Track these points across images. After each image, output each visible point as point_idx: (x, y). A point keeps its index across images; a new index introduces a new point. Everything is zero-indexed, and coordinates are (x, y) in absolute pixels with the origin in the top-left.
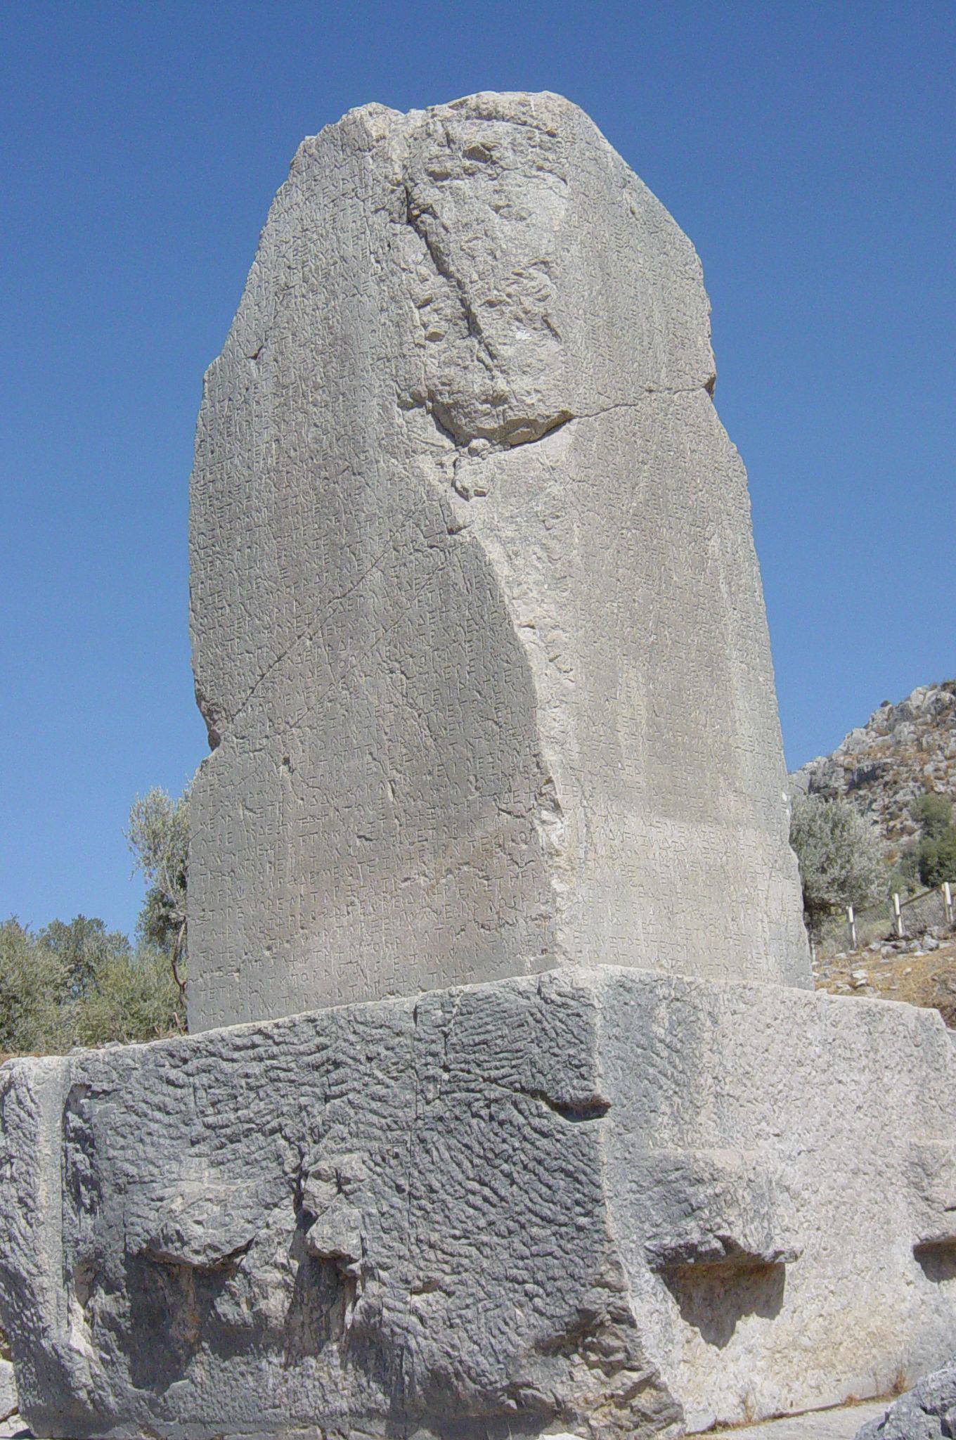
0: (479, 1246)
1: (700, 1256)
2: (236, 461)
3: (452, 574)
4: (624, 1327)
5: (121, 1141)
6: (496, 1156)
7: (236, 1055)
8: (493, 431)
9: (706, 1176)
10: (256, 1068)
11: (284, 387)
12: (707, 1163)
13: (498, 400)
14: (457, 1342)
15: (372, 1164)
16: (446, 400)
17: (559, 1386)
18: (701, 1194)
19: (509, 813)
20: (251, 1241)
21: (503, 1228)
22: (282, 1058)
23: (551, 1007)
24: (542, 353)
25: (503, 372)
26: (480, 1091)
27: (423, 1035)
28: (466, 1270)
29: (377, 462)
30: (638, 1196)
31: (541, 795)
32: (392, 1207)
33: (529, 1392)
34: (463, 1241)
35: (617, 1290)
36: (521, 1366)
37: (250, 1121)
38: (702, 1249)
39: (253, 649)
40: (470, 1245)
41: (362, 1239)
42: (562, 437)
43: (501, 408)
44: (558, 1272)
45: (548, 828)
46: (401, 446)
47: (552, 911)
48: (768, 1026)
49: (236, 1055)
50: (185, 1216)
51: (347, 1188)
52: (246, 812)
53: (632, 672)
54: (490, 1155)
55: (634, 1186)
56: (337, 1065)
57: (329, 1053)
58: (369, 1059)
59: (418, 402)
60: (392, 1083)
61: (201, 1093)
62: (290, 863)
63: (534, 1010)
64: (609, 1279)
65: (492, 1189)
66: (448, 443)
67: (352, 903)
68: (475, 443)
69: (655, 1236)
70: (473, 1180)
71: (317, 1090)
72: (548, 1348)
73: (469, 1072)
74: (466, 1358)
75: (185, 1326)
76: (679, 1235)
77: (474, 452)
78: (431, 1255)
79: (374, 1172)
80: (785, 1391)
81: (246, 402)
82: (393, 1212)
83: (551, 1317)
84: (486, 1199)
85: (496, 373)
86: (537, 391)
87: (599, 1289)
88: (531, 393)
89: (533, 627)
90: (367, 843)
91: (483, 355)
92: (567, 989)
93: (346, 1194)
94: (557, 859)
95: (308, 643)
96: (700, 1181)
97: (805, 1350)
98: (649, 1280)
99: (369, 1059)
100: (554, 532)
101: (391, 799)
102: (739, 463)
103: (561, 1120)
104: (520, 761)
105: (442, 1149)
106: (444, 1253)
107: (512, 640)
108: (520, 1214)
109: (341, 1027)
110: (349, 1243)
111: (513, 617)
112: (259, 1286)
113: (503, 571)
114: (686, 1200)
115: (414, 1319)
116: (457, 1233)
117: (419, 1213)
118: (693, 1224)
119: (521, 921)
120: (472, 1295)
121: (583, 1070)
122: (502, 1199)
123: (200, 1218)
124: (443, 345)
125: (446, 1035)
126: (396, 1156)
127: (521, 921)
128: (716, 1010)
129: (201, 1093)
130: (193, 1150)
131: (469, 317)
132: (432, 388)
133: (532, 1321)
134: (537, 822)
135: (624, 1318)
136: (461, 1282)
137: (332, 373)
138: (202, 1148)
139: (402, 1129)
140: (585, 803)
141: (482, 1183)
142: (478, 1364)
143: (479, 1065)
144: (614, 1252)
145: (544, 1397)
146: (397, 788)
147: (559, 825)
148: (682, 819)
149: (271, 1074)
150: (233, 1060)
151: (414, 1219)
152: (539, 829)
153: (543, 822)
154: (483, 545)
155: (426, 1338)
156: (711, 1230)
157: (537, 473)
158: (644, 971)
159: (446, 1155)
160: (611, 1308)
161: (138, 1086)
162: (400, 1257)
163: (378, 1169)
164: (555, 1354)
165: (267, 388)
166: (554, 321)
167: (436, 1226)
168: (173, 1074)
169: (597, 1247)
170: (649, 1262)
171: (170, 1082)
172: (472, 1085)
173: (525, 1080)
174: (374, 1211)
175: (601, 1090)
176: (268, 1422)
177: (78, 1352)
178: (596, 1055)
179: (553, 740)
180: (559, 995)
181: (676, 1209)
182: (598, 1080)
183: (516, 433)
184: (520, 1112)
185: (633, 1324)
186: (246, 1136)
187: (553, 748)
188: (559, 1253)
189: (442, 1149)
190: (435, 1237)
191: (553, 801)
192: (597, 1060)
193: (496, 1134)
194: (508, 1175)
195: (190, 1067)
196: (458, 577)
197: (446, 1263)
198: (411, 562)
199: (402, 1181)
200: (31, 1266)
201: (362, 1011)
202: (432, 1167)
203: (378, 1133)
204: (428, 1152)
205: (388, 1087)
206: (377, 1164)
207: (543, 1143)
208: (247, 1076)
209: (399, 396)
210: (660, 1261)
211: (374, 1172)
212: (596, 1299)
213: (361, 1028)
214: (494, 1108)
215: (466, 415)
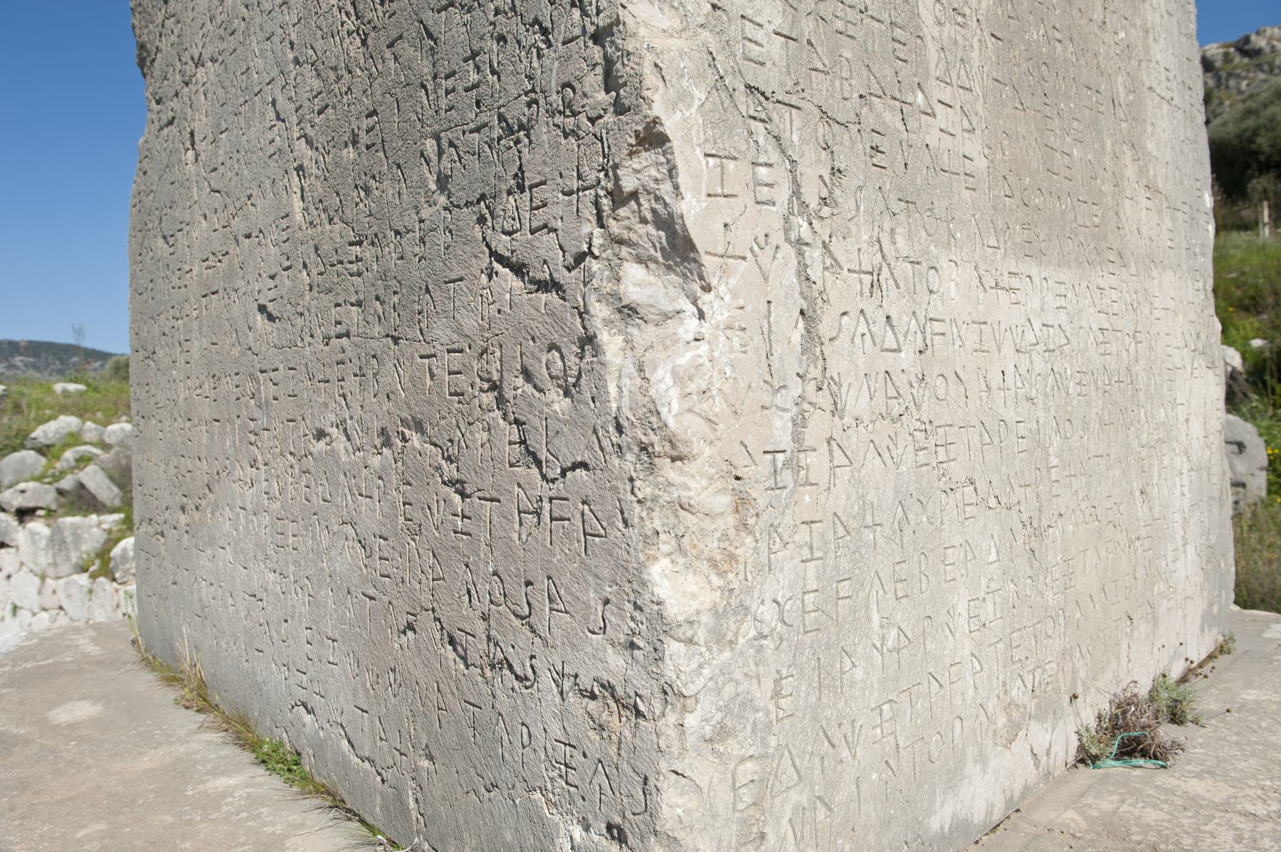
31: (619, 198)
45: (644, 335)
90: (269, 326)
94: (669, 471)
104: (552, 73)
134: (600, 311)
152: (611, 342)
153: (629, 312)
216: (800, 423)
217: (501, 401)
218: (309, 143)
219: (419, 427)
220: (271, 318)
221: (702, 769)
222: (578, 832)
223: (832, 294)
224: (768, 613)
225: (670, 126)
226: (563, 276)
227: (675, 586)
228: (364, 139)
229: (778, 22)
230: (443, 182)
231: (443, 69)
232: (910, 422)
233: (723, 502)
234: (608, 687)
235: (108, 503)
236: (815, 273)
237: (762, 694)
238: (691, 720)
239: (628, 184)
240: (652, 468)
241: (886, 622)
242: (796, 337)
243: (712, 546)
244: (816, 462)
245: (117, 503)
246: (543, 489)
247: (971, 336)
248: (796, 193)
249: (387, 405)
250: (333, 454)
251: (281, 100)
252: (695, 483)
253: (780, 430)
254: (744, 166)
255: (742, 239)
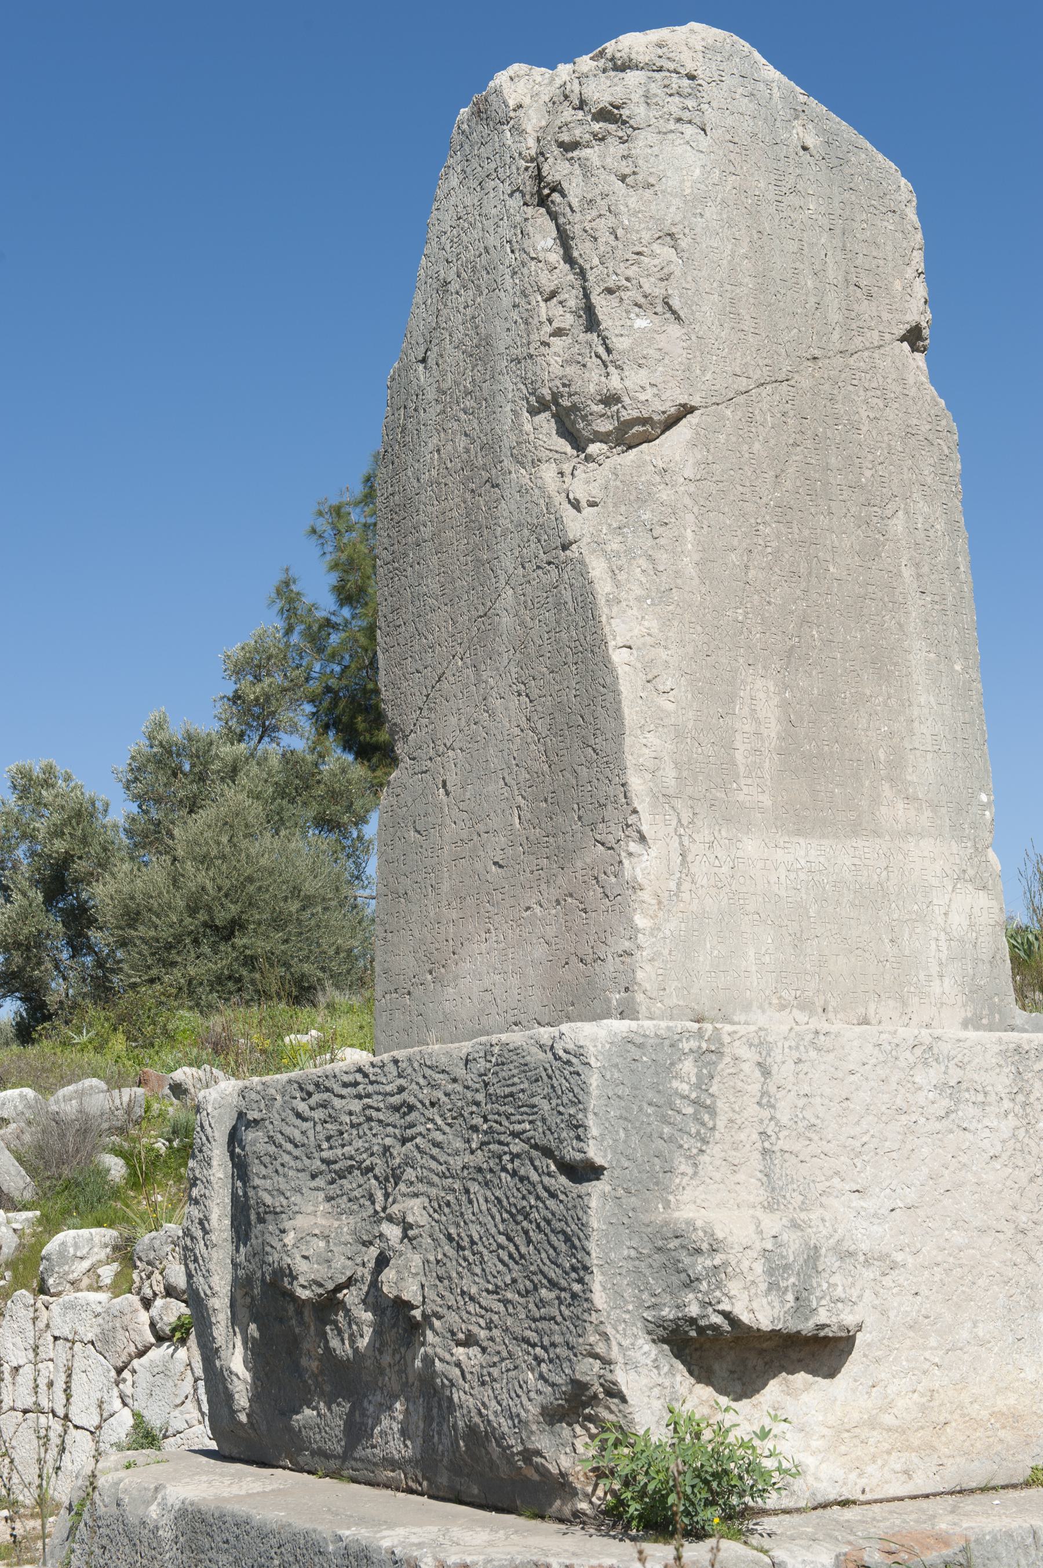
0: (506, 1302)
1: (701, 1330)
2: (410, 474)
3: (563, 592)
4: (616, 1401)
5: (264, 1171)
6: (518, 1211)
7: (344, 1091)
8: (608, 434)
9: (705, 1246)
10: (356, 1106)
11: (444, 393)
12: (705, 1232)
13: (610, 399)
14: (486, 1399)
15: (431, 1211)
16: (566, 403)
17: (562, 1457)
18: (701, 1264)
19: (603, 844)
20: (350, 1278)
21: (522, 1287)
22: (375, 1097)
23: (558, 1064)
24: (662, 341)
25: (617, 367)
26: (507, 1144)
27: (470, 1083)
28: (496, 1327)
29: (510, 473)
30: (637, 1262)
31: (628, 826)
32: (445, 1255)
33: (539, 1460)
34: (495, 1297)
35: (607, 1362)
36: (532, 1432)
37: (351, 1158)
38: (702, 1323)
39: (421, 668)
40: (499, 1301)
41: (423, 1286)
42: (682, 431)
43: (615, 408)
44: (558, 1339)
45: (634, 860)
46: (529, 454)
47: (634, 947)
48: (852, 1073)
49: (344, 1091)
50: (295, 1250)
51: (410, 1233)
52: (416, 835)
53: (759, 683)
54: (514, 1211)
55: (633, 1253)
56: (411, 1108)
57: (404, 1095)
58: (433, 1104)
59: (542, 406)
60: (447, 1129)
61: (319, 1128)
62: (445, 887)
63: (547, 1066)
64: (598, 1350)
65: (515, 1245)
66: (568, 449)
67: (488, 931)
68: (593, 448)
69: (654, 1306)
70: (503, 1234)
71: (397, 1131)
72: (552, 1416)
73: (501, 1125)
74: (492, 1417)
75: (310, 1357)
76: (678, 1307)
77: (589, 459)
78: (471, 1308)
79: (433, 1219)
80: (853, 1476)
81: (415, 410)
82: (445, 1260)
83: (553, 1385)
84: (511, 1256)
85: (611, 369)
86: (652, 385)
87: (591, 1360)
88: (645, 390)
89: (630, 647)
90: (499, 870)
91: (601, 350)
92: (570, 1047)
93: (410, 1240)
94: (639, 893)
95: (460, 663)
96: (698, 1251)
97: (889, 1430)
98: (646, 1350)
99: (433, 1104)
100: (662, 541)
101: (518, 826)
102: (947, 421)
103: (563, 1179)
105: (481, 1201)
106: (481, 1307)
107: (607, 663)
108: (534, 1273)
109: (414, 1070)
110: (411, 1292)
111: (609, 638)
112: (357, 1324)
113: (603, 587)
114: (685, 1271)
115: (457, 1371)
116: (490, 1287)
117: (464, 1264)
118: (691, 1296)
119: (610, 957)
120: (498, 1353)
121: (580, 1130)
122: (522, 1256)
123: (306, 1254)
124: (568, 340)
125: (486, 1084)
126: (448, 1204)
127: (610, 957)
128: (769, 1060)
129: (319, 1128)
130: (314, 1184)
131: (589, 309)
132: (555, 390)
133: (539, 1387)
134: (623, 854)
135: (614, 1392)
136: (492, 1339)
137: (478, 377)
138: (320, 1182)
139: (453, 1177)
140: (682, 831)
141: (510, 1239)
142: (499, 1424)
143: (508, 1118)
144: (602, 1322)
145: (550, 1467)
146: (522, 814)
147: (646, 857)
148: (823, 836)
149: (367, 1112)
150: (342, 1097)
151: (461, 1269)
152: (626, 862)
153: (630, 854)
154: (587, 560)
155: (465, 1393)
156: (710, 1304)
157: (648, 477)
158: (663, 1024)
159: (484, 1208)
160: (602, 1381)
161: (277, 1116)
162: (449, 1308)
163: (436, 1216)
164: (560, 1421)
165: (431, 394)
166: (676, 303)
167: (476, 1278)
168: (302, 1107)
169: (586, 1316)
170: (649, 1333)
171: (299, 1115)
172: (502, 1138)
173: (539, 1139)
174: (432, 1258)
175: (595, 1153)
176: (369, 1461)
177: (237, 1375)
178: (590, 1116)
179: (640, 768)
180: (565, 1051)
181: (675, 1280)
182: (591, 1142)
183: (629, 435)
184: (536, 1169)
185: (624, 1400)
186: (350, 1173)
187: (642, 777)
188: (559, 1319)
189: (481, 1201)
190: (474, 1290)
191: (639, 832)
192: (591, 1121)
193: (518, 1189)
194: (526, 1232)
195: (312, 1101)
196: (567, 595)
197: (482, 1317)
198: (534, 579)
199: (453, 1231)
200: (206, 1287)
201: (430, 1054)
202: (474, 1218)
203: (436, 1179)
204: (470, 1202)
205: (444, 1134)
206: (435, 1211)
207: (551, 1203)
208: (350, 1113)
209: (528, 402)
210: (661, 1332)
211: (433, 1219)
212: (588, 1370)
213: (429, 1072)
214: (517, 1162)
215: (584, 418)
216: (679, 884)
217: (598, 882)
218: (524, 798)
219: (571, 895)
220: (501, 866)
221: (648, 967)
222: (618, 996)
223: (693, 850)
224: (667, 932)
225: (638, 809)
226: (615, 846)
227: (640, 921)
228: (549, 800)
229: (674, 775)
230: (580, 818)
231: (580, 784)
232: (727, 889)
233: (654, 902)
234: (625, 952)
235: (16, 1195)
236: (686, 843)
237: (666, 952)
238: (644, 953)
239: (630, 823)
240: (635, 892)
241: (713, 948)
242: (678, 861)
243: (651, 912)
244: (686, 896)
245: (28, 1195)
246: (609, 904)
247: (760, 865)
248: (680, 821)
249: (558, 891)
250: (535, 914)
251: (507, 777)
252: (645, 896)
253: (672, 885)
254: (661, 816)
255: (660, 835)
